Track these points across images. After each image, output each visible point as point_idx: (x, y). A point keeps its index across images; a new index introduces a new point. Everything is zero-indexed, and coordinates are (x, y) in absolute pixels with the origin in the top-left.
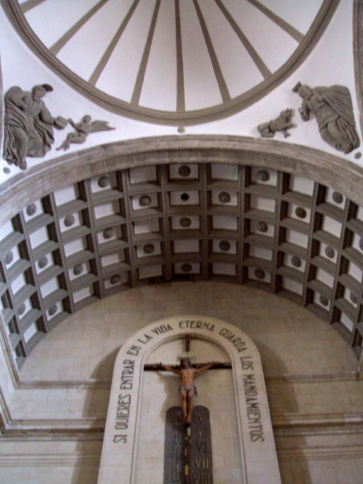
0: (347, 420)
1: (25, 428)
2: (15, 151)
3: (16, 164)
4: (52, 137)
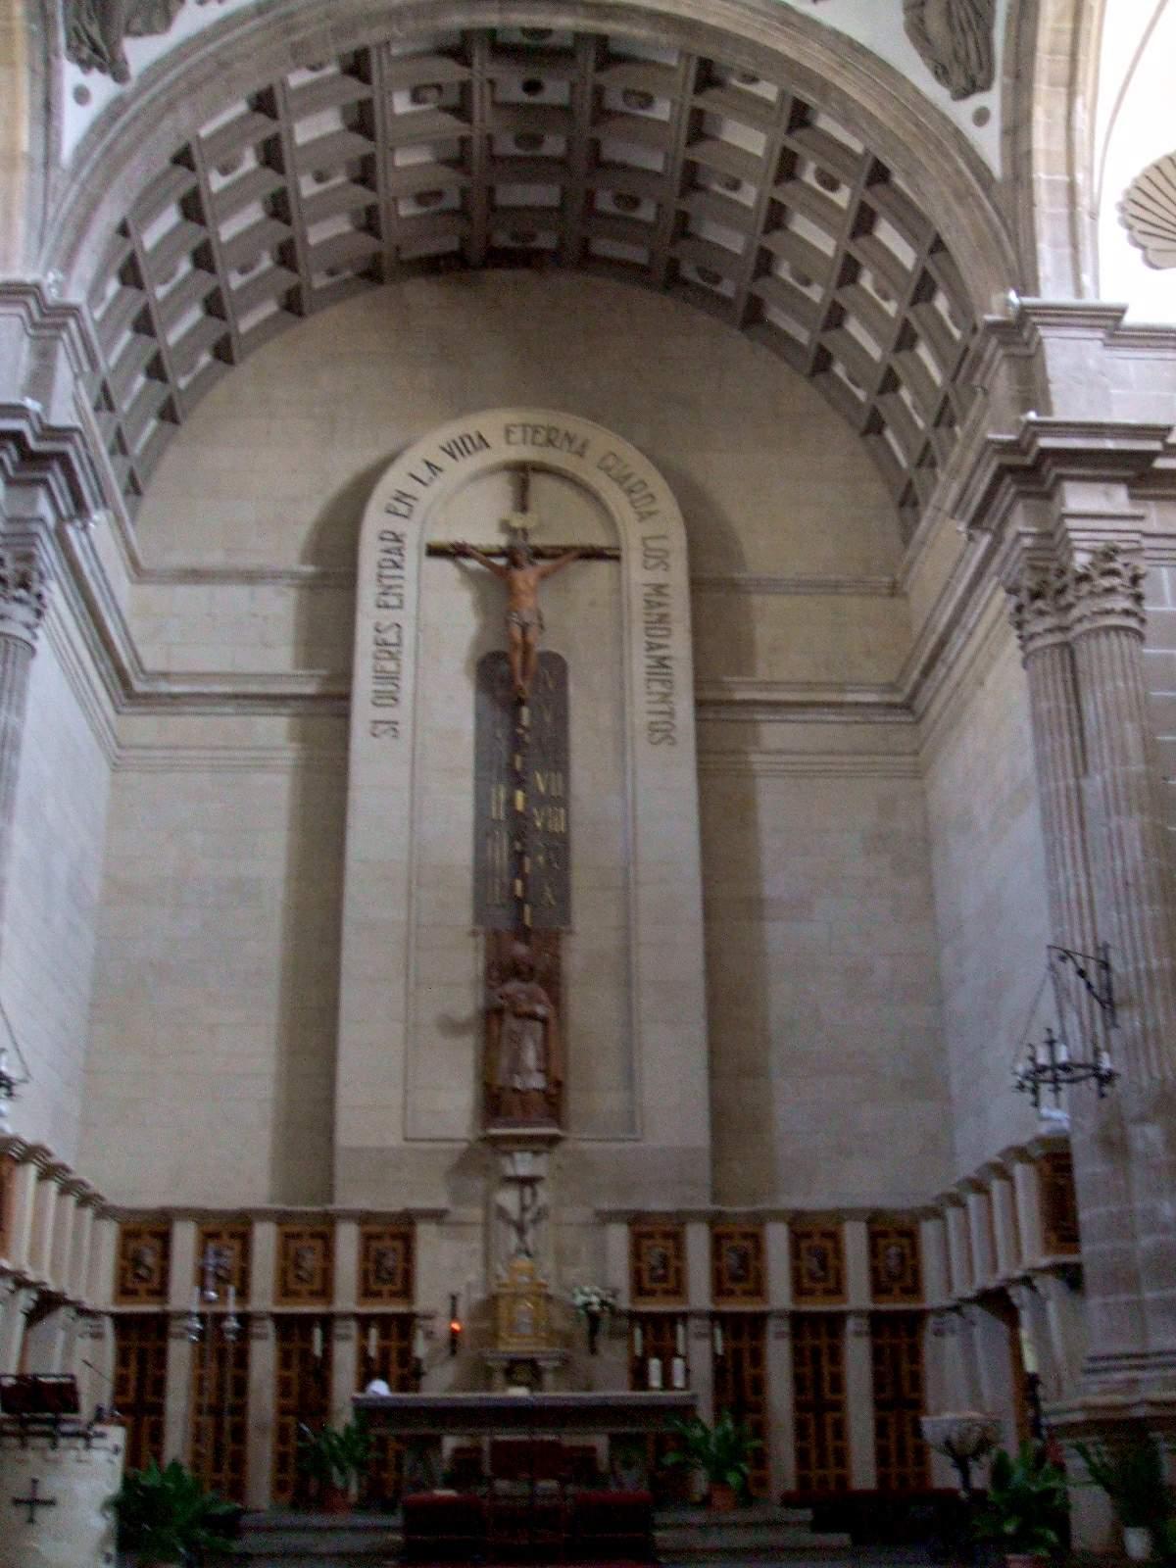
0: (850, 697)
1: (176, 689)
2: (94, 31)
3: (102, 69)
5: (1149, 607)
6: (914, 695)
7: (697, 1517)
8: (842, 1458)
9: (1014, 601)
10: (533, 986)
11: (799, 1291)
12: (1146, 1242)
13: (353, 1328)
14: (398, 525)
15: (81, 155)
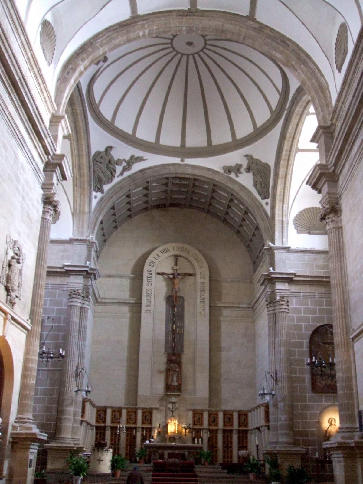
0: (241, 306)
2: (99, 186)
3: (99, 192)
4: (115, 171)
5: (290, 306)
6: (254, 305)
7: (203, 466)
8: (231, 457)
9: (266, 303)
10: (176, 365)
11: (225, 425)
12: (279, 423)
13: (140, 430)
14: (151, 268)
15: (95, 210)
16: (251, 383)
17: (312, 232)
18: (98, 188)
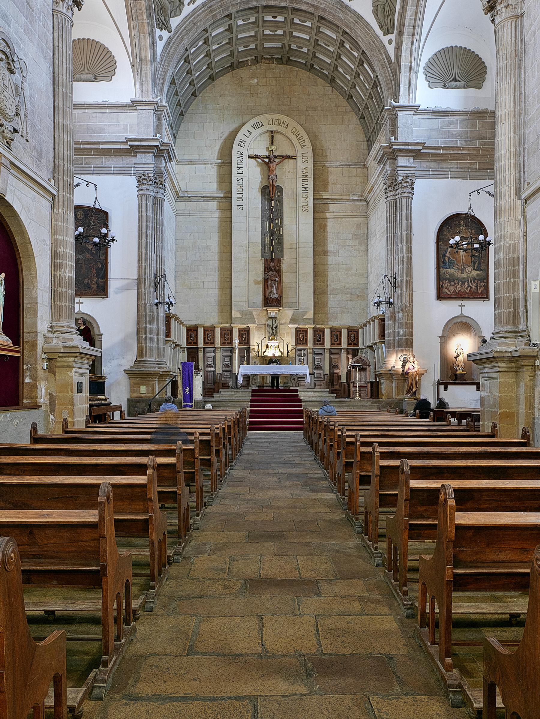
2: (163, 19)
11: (332, 344)
14: (241, 150)
16: (363, 295)
17: (448, 84)
18: (163, 24)
